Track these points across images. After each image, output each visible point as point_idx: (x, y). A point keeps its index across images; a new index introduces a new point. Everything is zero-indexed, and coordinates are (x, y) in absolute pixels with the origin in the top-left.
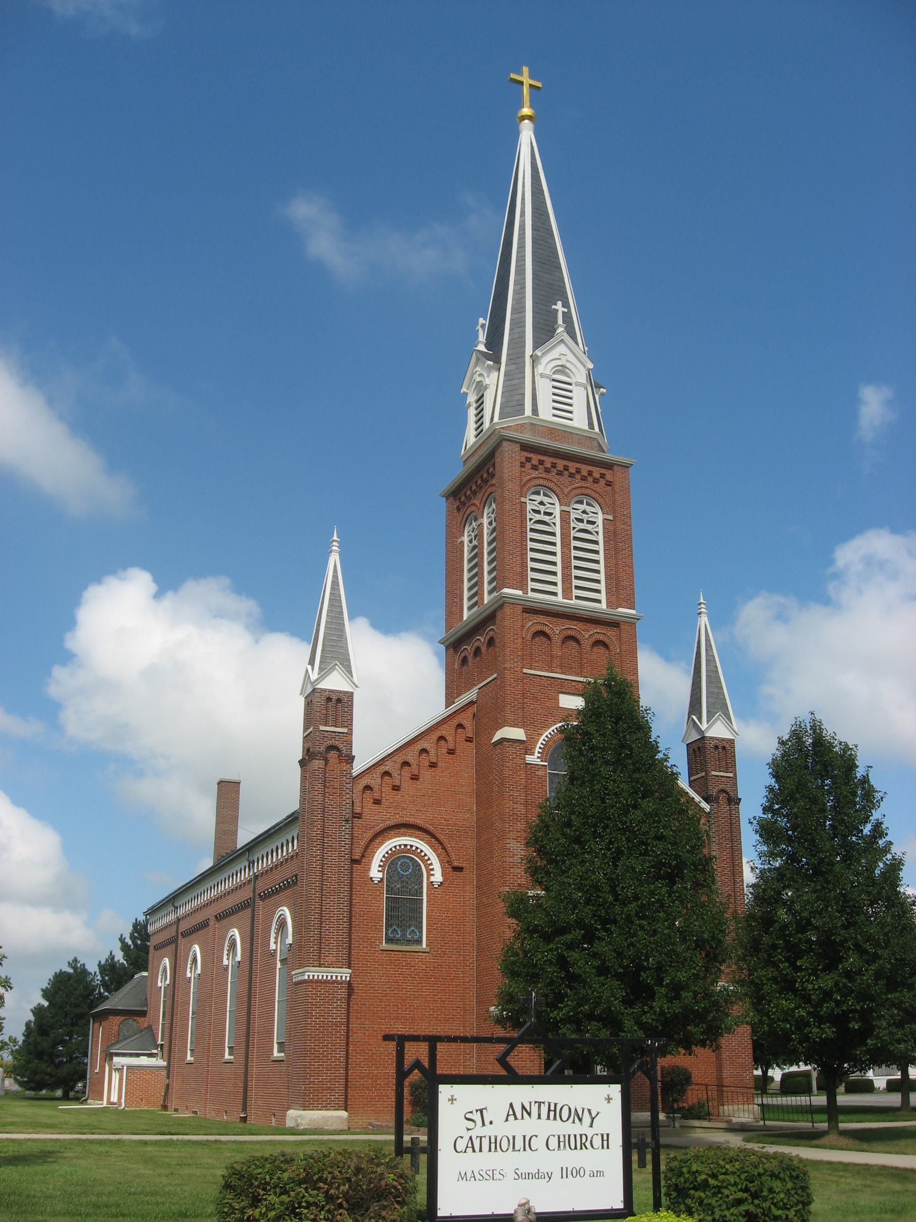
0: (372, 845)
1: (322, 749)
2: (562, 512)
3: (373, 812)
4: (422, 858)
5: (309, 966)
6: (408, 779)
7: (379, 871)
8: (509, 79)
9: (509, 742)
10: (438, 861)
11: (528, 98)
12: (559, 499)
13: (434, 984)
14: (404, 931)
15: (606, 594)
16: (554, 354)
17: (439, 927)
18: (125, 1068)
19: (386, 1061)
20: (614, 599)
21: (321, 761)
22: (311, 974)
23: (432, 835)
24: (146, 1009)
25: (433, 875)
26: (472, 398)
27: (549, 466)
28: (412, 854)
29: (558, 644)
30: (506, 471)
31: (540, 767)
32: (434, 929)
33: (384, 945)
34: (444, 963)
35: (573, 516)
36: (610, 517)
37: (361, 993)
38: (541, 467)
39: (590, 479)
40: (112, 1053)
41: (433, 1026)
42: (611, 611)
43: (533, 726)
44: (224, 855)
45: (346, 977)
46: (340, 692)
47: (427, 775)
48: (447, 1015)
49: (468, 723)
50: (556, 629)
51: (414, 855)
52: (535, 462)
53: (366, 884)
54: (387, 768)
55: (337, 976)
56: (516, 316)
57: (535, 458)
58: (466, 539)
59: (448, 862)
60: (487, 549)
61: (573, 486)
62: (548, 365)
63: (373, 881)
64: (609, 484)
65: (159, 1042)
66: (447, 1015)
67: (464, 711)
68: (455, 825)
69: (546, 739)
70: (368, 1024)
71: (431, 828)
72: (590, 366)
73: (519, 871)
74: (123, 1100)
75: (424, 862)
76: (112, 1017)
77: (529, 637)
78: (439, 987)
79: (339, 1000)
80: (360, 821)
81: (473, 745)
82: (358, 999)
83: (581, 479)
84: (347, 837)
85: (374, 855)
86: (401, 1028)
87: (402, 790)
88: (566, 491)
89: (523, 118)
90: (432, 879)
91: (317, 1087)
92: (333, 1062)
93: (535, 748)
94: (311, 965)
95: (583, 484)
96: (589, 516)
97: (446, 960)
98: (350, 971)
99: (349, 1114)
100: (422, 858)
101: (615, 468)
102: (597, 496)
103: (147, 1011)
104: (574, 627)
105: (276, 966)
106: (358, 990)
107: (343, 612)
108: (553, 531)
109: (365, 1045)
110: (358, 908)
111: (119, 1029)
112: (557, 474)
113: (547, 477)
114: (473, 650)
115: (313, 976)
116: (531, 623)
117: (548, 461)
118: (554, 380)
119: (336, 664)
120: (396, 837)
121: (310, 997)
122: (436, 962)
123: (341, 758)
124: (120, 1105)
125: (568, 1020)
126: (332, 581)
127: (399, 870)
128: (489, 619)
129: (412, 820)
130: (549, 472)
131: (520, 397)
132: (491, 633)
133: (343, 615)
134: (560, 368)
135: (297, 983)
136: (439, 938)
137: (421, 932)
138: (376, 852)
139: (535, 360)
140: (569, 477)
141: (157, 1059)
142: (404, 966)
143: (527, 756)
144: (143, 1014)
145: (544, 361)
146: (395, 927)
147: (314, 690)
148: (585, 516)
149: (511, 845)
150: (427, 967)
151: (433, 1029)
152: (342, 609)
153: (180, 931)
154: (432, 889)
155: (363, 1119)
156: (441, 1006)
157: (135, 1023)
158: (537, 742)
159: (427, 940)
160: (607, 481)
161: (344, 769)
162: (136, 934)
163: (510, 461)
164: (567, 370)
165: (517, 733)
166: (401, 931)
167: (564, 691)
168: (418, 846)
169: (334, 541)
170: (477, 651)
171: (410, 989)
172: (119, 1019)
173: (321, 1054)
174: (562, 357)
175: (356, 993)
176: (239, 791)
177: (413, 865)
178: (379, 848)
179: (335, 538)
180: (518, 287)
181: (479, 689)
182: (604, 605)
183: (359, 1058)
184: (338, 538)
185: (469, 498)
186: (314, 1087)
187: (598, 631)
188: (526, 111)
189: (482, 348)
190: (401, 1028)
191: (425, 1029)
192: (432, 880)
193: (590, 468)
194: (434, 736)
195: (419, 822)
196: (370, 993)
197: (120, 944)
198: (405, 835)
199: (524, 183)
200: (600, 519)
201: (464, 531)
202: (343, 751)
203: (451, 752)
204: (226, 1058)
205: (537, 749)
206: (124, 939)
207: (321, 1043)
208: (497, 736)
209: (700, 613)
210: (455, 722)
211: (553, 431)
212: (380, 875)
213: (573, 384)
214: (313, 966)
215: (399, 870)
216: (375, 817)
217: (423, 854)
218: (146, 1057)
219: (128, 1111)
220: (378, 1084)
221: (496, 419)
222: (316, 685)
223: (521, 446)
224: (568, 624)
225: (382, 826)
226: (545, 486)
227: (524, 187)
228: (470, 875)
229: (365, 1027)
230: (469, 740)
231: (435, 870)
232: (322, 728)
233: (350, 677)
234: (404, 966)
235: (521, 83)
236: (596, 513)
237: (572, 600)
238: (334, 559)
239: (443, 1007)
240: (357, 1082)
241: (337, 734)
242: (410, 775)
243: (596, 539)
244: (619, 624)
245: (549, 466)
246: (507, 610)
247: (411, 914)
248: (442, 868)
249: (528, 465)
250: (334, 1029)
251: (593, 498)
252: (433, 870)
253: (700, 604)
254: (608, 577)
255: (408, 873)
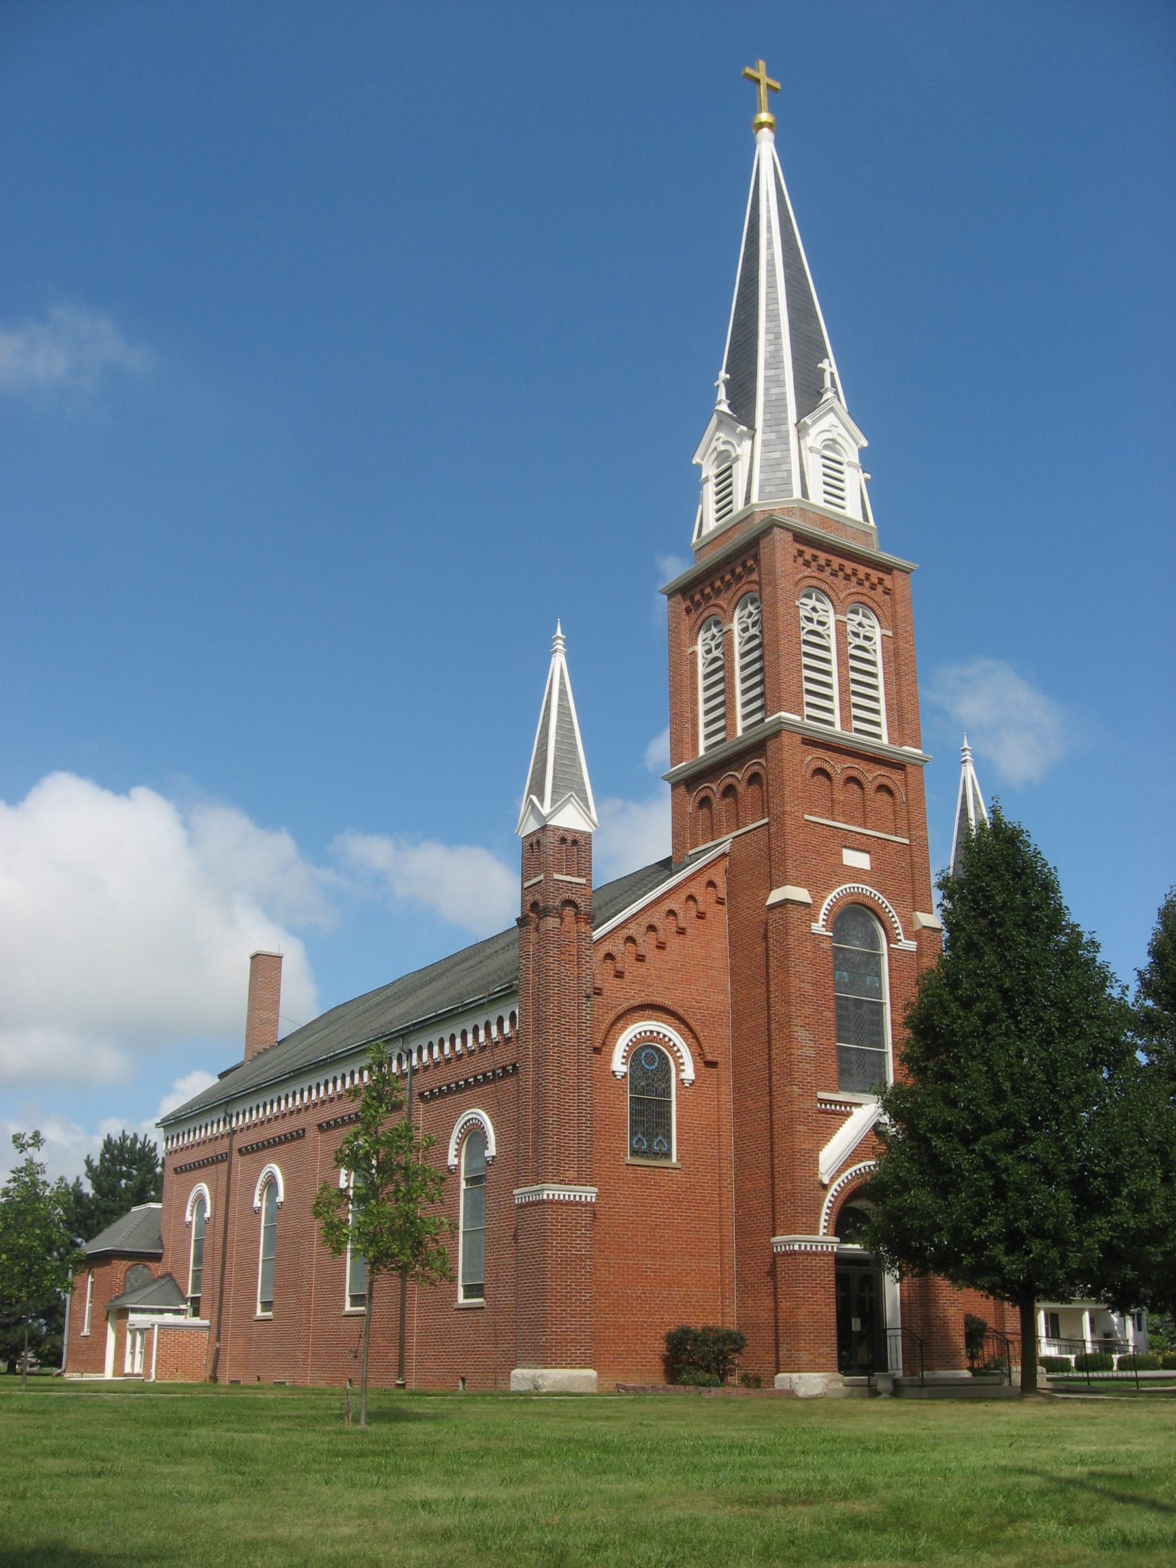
0: (613, 1030)
1: (557, 903)
2: (838, 623)
3: (614, 987)
4: (670, 1048)
5: (549, 1183)
6: (653, 947)
7: (623, 1063)
8: (742, 74)
9: (793, 904)
10: (689, 1053)
11: (766, 100)
12: (833, 606)
13: (686, 1209)
14: (650, 1141)
15: (888, 728)
16: (825, 423)
17: (692, 1137)
18: (156, 1327)
19: (634, 1307)
20: (896, 735)
21: (556, 919)
22: (551, 1193)
23: (682, 1020)
24: (161, 1251)
25: (683, 1071)
26: (709, 471)
27: (823, 563)
28: (659, 1043)
29: (840, 786)
30: (778, 565)
31: (825, 938)
32: (685, 1139)
33: (629, 1159)
34: (697, 1182)
35: (849, 628)
36: (890, 634)
37: (605, 1219)
38: (813, 564)
39: (867, 584)
40: (127, 1309)
41: (687, 1262)
42: (895, 748)
43: (819, 887)
44: (262, 1051)
45: (591, 1197)
46: (576, 832)
47: (674, 943)
48: (702, 1249)
49: (721, 881)
50: (839, 766)
51: (661, 1044)
52: (808, 557)
53: (608, 1079)
54: (631, 931)
55: (580, 1196)
56: (772, 372)
57: (809, 552)
58: (700, 649)
59: (699, 1055)
60: (739, 662)
61: (849, 591)
62: (823, 434)
63: (616, 1076)
64: (887, 592)
65: (189, 1295)
66: (702, 1249)
67: (715, 864)
68: (708, 1008)
69: (831, 904)
70: (612, 1259)
71: (681, 1011)
72: (865, 443)
73: (808, 1066)
74: (153, 1370)
75: (673, 1053)
76: (116, 1262)
77: (808, 775)
78: (693, 1213)
79: (583, 1227)
80: (600, 998)
81: (725, 908)
82: (601, 1226)
83: (857, 583)
84: (588, 1018)
85: (616, 1043)
86: (650, 1264)
87: (647, 961)
88: (842, 596)
89: (761, 125)
90: (683, 1076)
91: (561, 1339)
92: (577, 1307)
93: (819, 914)
94: (550, 1181)
95: (859, 589)
96: (866, 629)
97: (699, 1179)
98: (596, 1190)
99: (598, 1373)
100: (670, 1048)
101: (895, 572)
102: (874, 605)
103: (162, 1254)
104: (857, 766)
105: (459, 1186)
106: (601, 1215)
107: (573, 729)
108: (827, 645)
109: (609, 1285)
110: (599, 1110)
111: (125, 1278)
112: (832, 574)
113: (820, 577)
114: (721, 788)
115: (554, 1195)
116: (810, 757)
117: (823, 557)
118: (824, 457)
119: (572, 796)
120: (640, 1021)
121: (549, 1222)
122: (688, 1182)
123: (579, 916)
124: (149, 1376)
125: (995, 1239)
126: (560, 689)
127: (644, 1063)
128: (757, 748)
129: (659, 1000)
130: (822, 571)
131: (785, 474)
132: (755, 768)
133: (574, 733)
134: (830, 442)
135: (521, 1206)
136: (692, 1151)
137: (670, 1143)
138: (617, 1039)
139: (802, 430)
140: (845, 579)
141: (186, 1317)
142: (652, 1185)
143: (812, 924)
144: (157, 1258)
145: (813, 431)
146: (639, 1135)
147: (544, 828)
148: (860, 630)
149: (799, 1034)
150: (679, 1188)
151: (687, 1266)
152: (572, 725)
153: (236, 1147)
154: (683, 1088)
155: (609, 1380)
156: (695, 1238)
157: (146, 1271)
158: (821, 907)
159: (677, 1153)
160: (886, 588)
161: (583, 931)
162: (107, 1156)
163: (783, 553)
164: (838, 446)
165: (801, 894)
166: (647, 1141)
167: (848, 844)
168: (666, 1033)
169: (558, 638)
170: (729, 791)
171: (660, 1215)
172: (125, 1265)
173: (564, 1296)
174: (833, 428)
175: (599, 1218)
176: (281, 968)
177: (659, 1057)
178: (621, 1034)
179: (559, 633)
180: (772, 336)
181: (733, 838)
182: (885, 740)
183: (604, 1303)
184: (562, 634)
185: (707, 598)
186: (557, 1339)
187: (883, 773)
188: (764, 117)
189: (724, 407)
190: (650, 1264)
191: (677, 1266)
192: (683, 1077)
193: (868, 570)
194: (683, 895)
195: (667, 1003)
196: (614, 1219)
197: (85, 1168)
198: (650, 1019)
199: (768, 206)
200: (877, 634)
201: (697, 639)
202: (581, 907)
203: (701, 916)
204: (346, 1310)
205: (822, 916)
206: (92, 1161)
207: (564, 1282)
208: (775, 896)
209: (965, 761)
210: (705, 878)
211: (825, 520)
212: (625, 1069)
213: (845, 464)
214: (552, 1183)
215: (644, 1063)
216: (620, 994)
217: (671, 1044)
218: (171, 1315)
219: (157, 1384)
220: (626, 1336)
221: (755, 499)
222: (548, 821)
223: (794, 535)
224: (850, 762)
225: (626, 1006)
226: (819, 589)
227: (768, 211)
228: (726, 1073)
229: (609, 1263)
230: (720, 902)
231: (686, 1064)
232: (557, 876)
233: (588, 812)
234: (652, 1185)
235: (758, 81)
236: (873, 627)
237: (851, 732)
238: (559, 662)
239: (698, 1238)
240: (601, 1332)
241: (574, 885)
242: (655, 943)
243: (872, 659)
244: (905, 766)
245: (823, 563)
246: (785, 738)
247: (657, 1119)
248: (694, 1062)
249: (800, 560)
250: (578, 1265)
251: (870, 608)
252: (683, 1064)
253: (964, 750)
254: (889, 708)
255: (653, 1067)
